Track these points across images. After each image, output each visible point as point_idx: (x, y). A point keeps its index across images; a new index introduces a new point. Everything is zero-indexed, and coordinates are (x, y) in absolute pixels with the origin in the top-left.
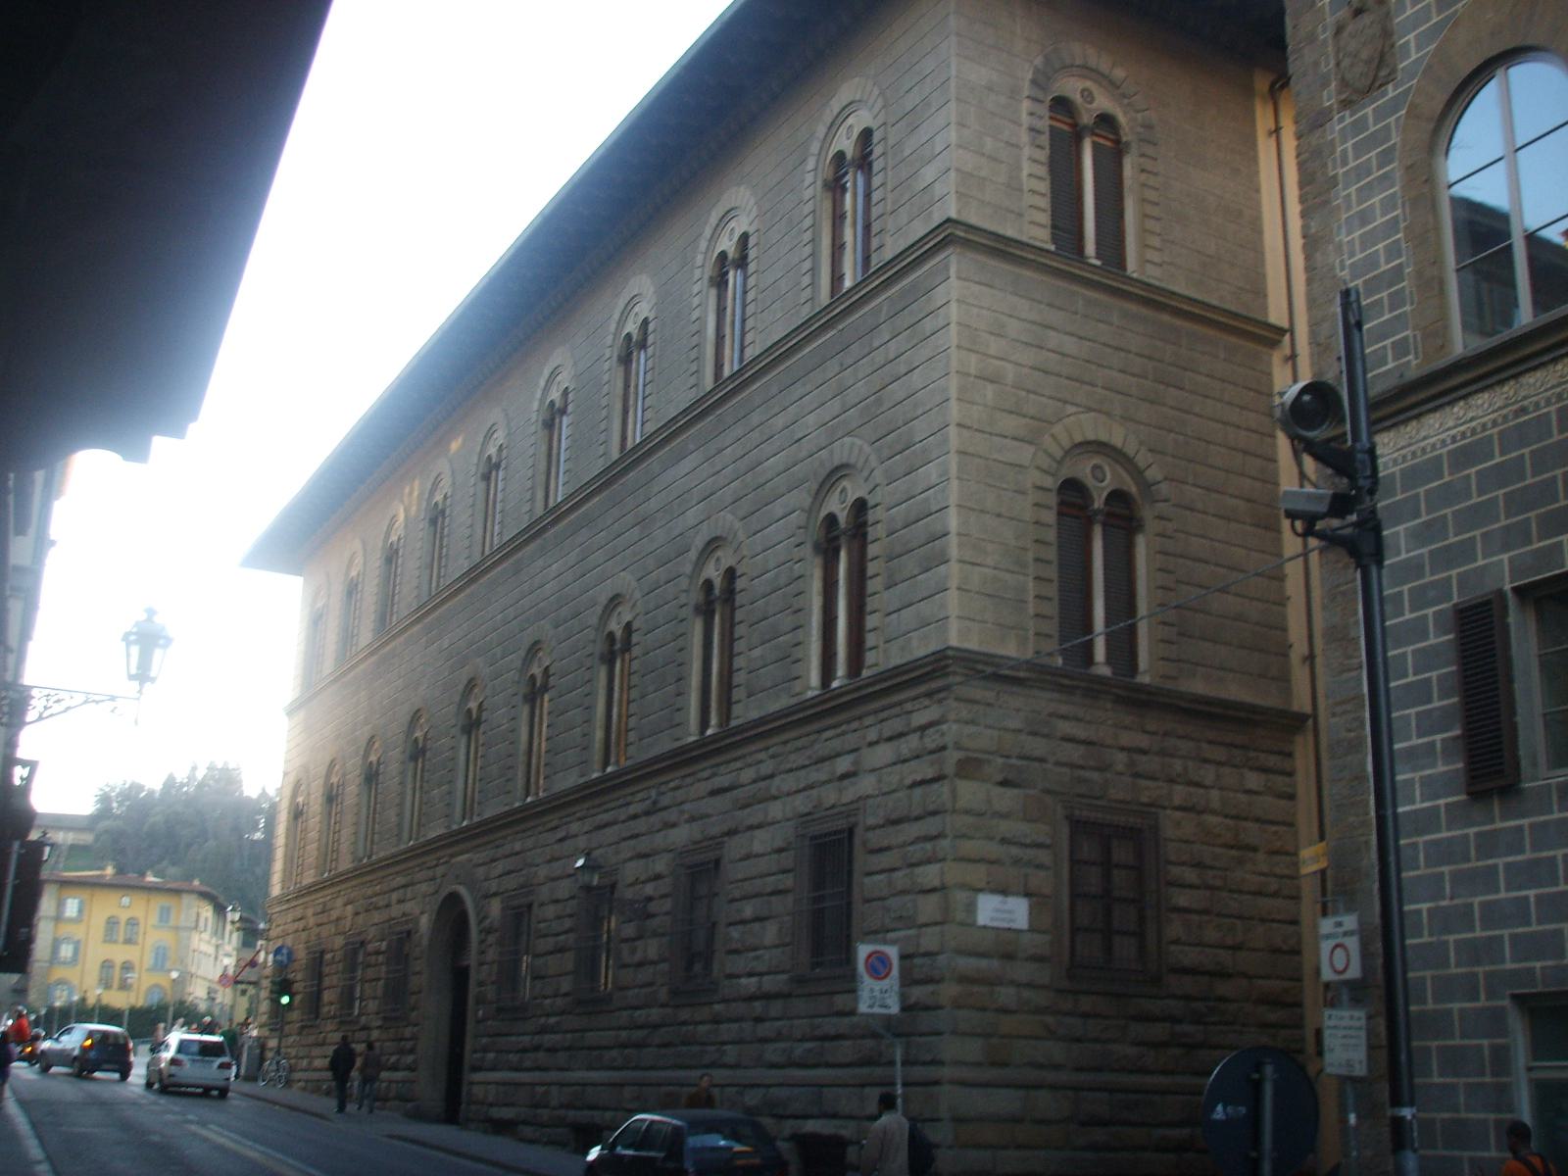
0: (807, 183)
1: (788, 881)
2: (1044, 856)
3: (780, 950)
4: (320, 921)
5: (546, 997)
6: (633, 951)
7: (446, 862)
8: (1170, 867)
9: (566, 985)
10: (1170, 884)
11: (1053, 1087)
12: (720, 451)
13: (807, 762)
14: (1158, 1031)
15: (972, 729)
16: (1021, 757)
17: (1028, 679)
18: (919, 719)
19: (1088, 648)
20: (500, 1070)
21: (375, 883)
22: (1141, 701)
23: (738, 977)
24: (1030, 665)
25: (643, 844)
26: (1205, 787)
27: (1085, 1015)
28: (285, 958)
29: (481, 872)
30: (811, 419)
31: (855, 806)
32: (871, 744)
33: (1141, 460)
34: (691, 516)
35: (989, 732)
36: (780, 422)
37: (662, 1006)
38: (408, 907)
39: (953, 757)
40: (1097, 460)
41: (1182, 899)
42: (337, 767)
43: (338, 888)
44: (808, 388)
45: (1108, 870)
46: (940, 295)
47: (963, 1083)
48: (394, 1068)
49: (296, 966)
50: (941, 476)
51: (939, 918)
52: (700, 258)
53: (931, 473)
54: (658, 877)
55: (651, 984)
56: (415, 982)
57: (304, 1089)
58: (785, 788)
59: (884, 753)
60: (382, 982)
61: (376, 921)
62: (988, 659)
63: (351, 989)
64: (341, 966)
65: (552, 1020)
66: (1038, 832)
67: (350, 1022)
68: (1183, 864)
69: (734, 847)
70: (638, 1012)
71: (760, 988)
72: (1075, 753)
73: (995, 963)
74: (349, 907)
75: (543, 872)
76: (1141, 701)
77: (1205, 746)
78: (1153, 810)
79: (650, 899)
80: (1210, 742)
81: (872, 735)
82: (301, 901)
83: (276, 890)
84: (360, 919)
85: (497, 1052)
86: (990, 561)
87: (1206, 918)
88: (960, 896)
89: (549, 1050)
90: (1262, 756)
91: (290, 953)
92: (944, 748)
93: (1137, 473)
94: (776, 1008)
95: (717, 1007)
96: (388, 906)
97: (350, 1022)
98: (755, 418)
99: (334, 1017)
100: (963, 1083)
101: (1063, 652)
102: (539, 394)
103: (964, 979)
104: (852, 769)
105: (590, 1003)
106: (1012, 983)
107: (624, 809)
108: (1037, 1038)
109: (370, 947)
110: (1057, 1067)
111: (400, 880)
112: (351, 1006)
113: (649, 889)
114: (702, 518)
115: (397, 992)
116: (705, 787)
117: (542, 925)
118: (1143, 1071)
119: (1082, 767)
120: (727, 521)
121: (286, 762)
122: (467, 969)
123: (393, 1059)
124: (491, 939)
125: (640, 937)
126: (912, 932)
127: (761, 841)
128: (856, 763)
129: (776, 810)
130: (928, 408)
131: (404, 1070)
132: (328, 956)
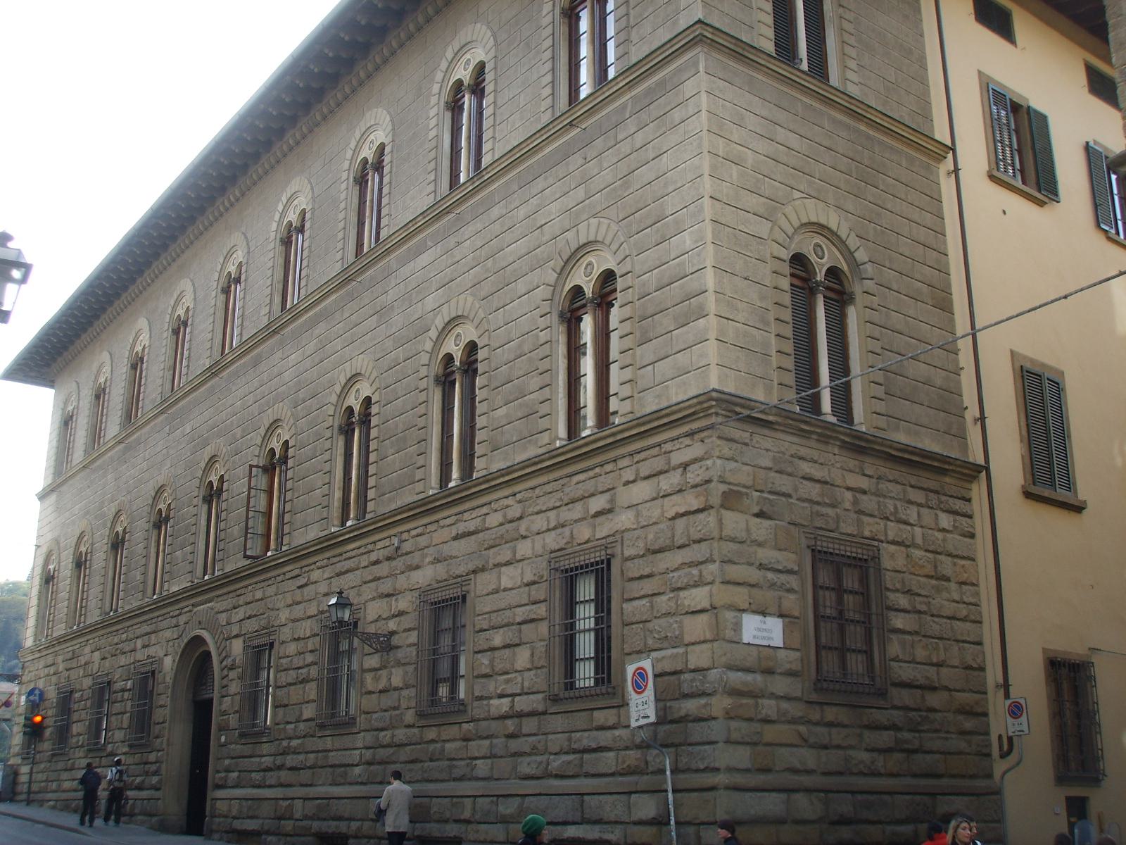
0: (544, 12)
1: (542, 610)
2: (793, 581)
3: (533, 672)
4: (69, 666)
5: (288, 723)
6: (377, 679)
7: (190, 611)
8: (888, 593)
9: (309, 712)
10: (889, 608)
11: (808, 790)
12: (459, 244)
13: (558, 504)
14: (886, 738)
15: (733, 465)
16: (770, 492)
17: (777, 423)
18: (677, 458)
19: (816, 399)
20: (244, 787)
21: (121, 632)
22: (860, 446)
23: (491, 698)
24: (779, 410)
25: (386, 587)
26: (911, 525)
27: (831, 725)
28: (37, 698)
29: (223, 618)
30: (554, 207)
31: (611, 539)
32: (627, 483)
33: (853, 242)
34: (430, 302)
35: (746, 468)
36: (522, 212)
37: (408, 726)
38: (151, 651)
39: (718, 489)
40: (818, 240)
41: (899, 621)
42: (85, 539)
43: (85, 638)
44: (551, 181)
45: (844, 590)
46: (689, 88)
47: (737, 789)
48: (139, 788)
49: (47, 704)
50: (696, 241)
51: (708, 636)
52: (436, 88)
53: (687, 239)
54: (401, 614)
55: (395, 708)
56: (158, 715)
57: (54, 808)
58: (535, 528)
59: (642, 491)
60: (128, 714)
61: (122, 664)
62: (747, 402)
63: (99, 721)
64: (89, 703)
65: (294, 743)
66: (786, 559)
67: (99, 750)
68: (897, 591)
69: (483, 583)
70: (383, 734)
71: (512, 707)
72: (813, 491)
73: (759, 678)
74: (97, 654)
75: (284, 616)
76: (860, 446)
77: (909, 489)
78: (876, 543)
79: (393, 633)
80: (912, 486)
81: (629, 475)
82: (50, 651)
83: (29, 643)
84: (107, 663)
85: (240, 771)
86: (740, 317)
87: (917, 638)
88: (729, 615)
89: (291, 769)
90: (951, 500)
91: (42, 694)
92: (708, 481)
93: (849, 254)
94: (529, 725)
95: (465, 726)
96: (134, 650)
97: (99, 750)
98: (496, 212)
99: (82, 746)
100: (737, 789)
101: (800, 402)
102: (277, 217)
103: (735, 692)
104: (608, 506)
105: (334, 721)
106: (773, 696)
107: (365, 556)
108: (796, 746)
109: (118, 686)
110: (809, 772)
111: (146, 628)
112: (98, 736)
113: (392, 625)
114: (442, 301)
115: (143, 722)
116: (446, 534)
117: (284, 661)
118: (875, 774)
119: (818, 503)
120: (466, 303)
121: (38, 537)
122: (210, 702)
123: (138, 780)
124: (233, 674)
125: (383, 667)
126: (681, 650)
127: (508, 577)
128: (612, 501)
129: (524, 548)
130: (679, 185)
131: (148, 789)
132: (77, 695)
